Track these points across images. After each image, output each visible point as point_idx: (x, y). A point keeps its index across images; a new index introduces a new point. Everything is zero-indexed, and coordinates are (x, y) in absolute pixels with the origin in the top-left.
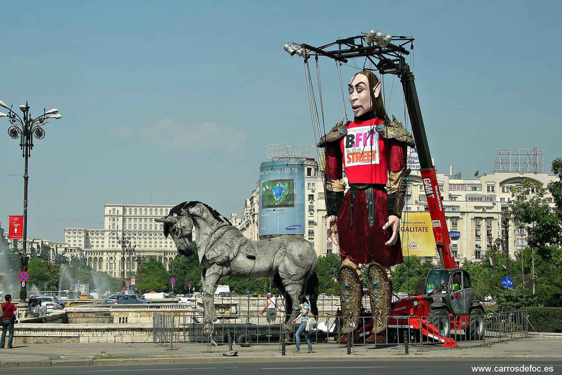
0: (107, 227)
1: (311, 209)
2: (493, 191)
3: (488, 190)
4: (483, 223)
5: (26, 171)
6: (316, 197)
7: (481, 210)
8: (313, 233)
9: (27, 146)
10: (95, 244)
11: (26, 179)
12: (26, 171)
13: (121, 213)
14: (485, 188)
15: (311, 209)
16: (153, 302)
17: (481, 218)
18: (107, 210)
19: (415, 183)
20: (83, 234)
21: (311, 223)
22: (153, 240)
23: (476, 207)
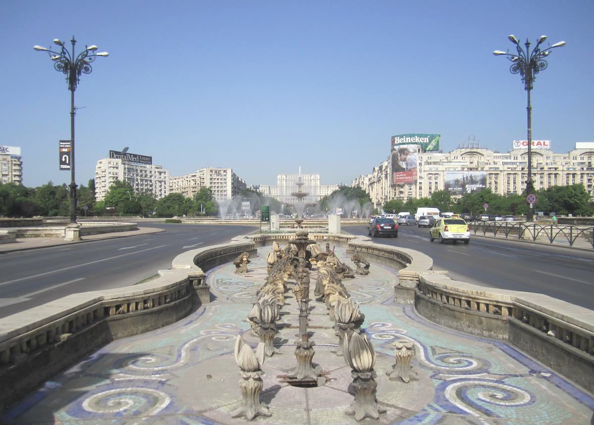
0: (278, 185)
1: (421, 171)
2: (517, 159)
3: (514, 159)
4: (512, 177)
5: (529, 102)
6: (423, 164)
7: (510, 169)
8: (491, 183)
9: (73, 82)
10: (273, 193)
11: (529, 109)
12: (529, 102)
13: (285, 178)
14: (513, 157)
15: (421, 171)
16: (559, 254)
17: (511, 174)
18: (279, 177)
19: (475, 156)
20: (268, 188)
21: (421, 177)
22: (324, 191)
23: (508, 168)
